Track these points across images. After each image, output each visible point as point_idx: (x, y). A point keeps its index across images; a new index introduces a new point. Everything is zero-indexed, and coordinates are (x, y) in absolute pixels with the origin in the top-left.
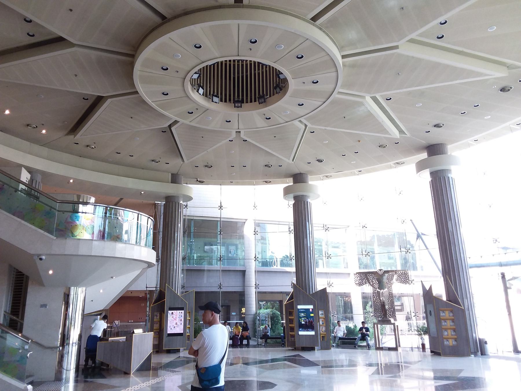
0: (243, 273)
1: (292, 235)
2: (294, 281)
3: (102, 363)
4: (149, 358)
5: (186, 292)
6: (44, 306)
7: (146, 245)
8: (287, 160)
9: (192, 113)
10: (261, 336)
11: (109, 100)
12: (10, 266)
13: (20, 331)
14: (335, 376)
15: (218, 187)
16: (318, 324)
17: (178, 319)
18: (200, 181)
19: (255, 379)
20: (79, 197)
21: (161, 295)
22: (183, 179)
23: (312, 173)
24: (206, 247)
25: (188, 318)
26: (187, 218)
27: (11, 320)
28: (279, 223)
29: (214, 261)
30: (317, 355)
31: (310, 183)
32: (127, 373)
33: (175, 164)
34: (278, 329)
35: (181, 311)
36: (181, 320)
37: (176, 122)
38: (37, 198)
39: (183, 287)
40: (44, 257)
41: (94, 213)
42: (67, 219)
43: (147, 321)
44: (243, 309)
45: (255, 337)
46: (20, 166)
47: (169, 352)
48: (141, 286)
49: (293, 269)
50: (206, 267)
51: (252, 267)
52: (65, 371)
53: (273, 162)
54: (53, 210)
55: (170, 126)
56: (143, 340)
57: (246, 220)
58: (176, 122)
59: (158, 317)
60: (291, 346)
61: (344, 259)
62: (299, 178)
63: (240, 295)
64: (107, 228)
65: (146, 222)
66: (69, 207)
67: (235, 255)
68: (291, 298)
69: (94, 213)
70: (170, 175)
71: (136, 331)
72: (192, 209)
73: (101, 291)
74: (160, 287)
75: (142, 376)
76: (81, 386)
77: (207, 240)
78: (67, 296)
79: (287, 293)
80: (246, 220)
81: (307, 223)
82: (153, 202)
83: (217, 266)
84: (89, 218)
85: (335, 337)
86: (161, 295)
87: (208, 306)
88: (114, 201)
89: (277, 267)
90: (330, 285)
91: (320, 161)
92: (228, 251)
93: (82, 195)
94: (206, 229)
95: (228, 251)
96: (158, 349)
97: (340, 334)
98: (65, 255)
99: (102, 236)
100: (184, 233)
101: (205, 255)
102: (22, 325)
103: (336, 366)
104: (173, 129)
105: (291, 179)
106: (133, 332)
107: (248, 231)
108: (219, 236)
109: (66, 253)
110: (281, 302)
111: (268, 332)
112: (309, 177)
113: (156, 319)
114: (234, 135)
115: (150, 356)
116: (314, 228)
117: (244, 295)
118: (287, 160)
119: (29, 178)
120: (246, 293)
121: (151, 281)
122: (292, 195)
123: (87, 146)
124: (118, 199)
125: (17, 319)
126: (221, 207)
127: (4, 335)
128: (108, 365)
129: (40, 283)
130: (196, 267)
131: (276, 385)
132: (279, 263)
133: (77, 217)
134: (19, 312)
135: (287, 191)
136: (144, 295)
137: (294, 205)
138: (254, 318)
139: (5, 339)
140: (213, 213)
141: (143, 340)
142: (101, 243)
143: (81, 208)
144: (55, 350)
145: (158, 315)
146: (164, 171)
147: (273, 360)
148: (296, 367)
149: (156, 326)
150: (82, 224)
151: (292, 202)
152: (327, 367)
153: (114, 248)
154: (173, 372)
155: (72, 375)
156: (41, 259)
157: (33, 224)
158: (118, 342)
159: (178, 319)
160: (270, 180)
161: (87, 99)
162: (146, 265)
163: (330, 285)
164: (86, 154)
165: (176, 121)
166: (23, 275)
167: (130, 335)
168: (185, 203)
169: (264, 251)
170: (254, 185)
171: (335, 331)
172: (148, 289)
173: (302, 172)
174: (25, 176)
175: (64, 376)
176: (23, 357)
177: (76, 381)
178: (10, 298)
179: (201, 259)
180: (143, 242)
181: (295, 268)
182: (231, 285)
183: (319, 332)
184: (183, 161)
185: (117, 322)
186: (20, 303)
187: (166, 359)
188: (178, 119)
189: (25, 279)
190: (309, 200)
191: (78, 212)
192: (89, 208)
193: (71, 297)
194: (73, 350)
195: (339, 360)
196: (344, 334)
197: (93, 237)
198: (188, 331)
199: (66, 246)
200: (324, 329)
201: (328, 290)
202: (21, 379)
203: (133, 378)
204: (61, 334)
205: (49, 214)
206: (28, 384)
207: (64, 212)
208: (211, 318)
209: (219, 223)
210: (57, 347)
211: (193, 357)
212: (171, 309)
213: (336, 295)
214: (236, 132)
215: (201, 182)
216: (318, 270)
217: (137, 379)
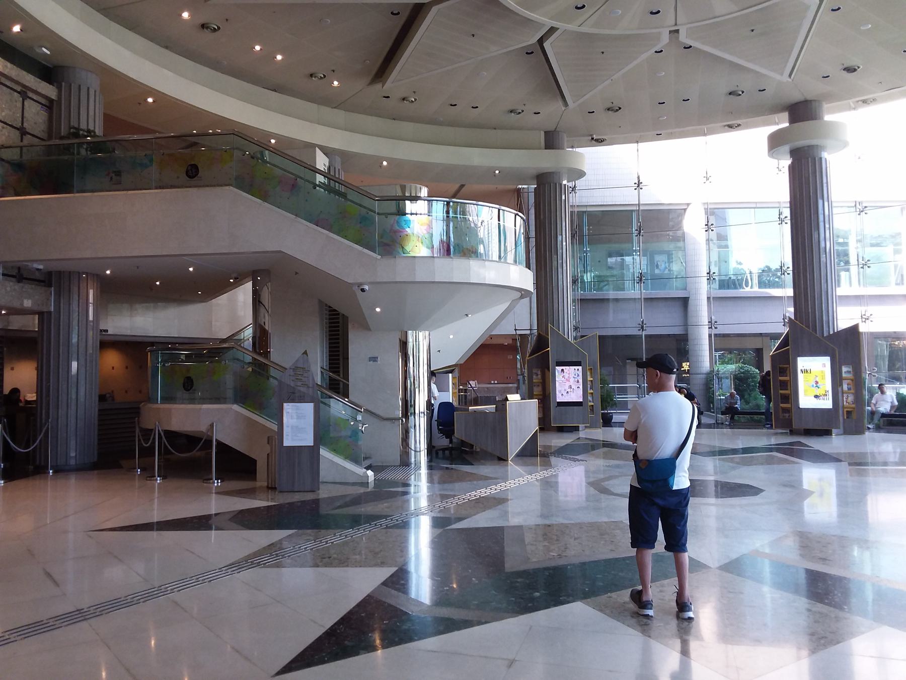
0: (684, 302)
1: (787, 228)
2: (790, 311)
3: (463, 443)
4: (534, 438)
5: (582, 336)
6: (374, 359)
7: (515, 261)
8: (777, 77)
9: (584, 6)
10: (723, 409)
11: (434, 10)
12: (320, 302)
13: (346, 395)
14: (870, 479)
15: (633, 146)
16: (840, 389)
17: (572, 380)
18: (597, 140)
19: (712, 478)
20: (403, 188)
21: (541, 342)
22: (566, 139)
23: (830, 97)
24: (609, 260)
25: (589, 378)
26: (576, 210)
27: (331, 379)
28: (756, 206)
29: (628, 284)
30: (836, 443)
31: (827, 118)
32: (502, 459)
33: (551, 112)
34: (756, 399)
35: (577, 368)
36: (578, 382)
37: (552, 30)
38: (343, 195)
39: (576, 328)
40: (366, 287)
41: (429, 213)
42: (392, 226)
43: (521, 382)
44: (684, 364)
45: (709, 410)
46: (312, 147)
47: (561, 430)
48: (507, 329)
49: (790, 292)
50: (612, 294)
51: (702, 291)
52: (413, 453)
53: (745, 83)
54: (370, 213)
55: (541, 41)
56: (521, 412)
57: (688, 204)
58: (552, 30)
59: (539, 376)
60: (782, 427)
61: (896, 267)
62: (802, 111)
63: (677, 340)
64: (452, 236)
65: (513, 221)
66: (392, 206)
67: (666, 272)
68: (785, 343)
69: (429, 213)
70: (543, 133)
71: (510, 397)
72: (584, 193)
73: (451, 337)
74: (538, 329)
75: (525, 464)
76: (437, 474)
77: (616, 246)
78: (404, 345)
79: (774, 337)
80: (688, 204)
81: (820, 202)
82: (514, 187)
83: (633, 292)
84: (423, 221)
85: (873, 413)
86: (541, 342)
87: (662, 359)
88: (457, 190)
89: (753, 289)
90: (865, 319)
91: (850, 70)
92: (653, 264)
93: (408, 186)
94: (611, 228)
95: (653, 264)
96: (545, 425)
97: (885, 407)
98: (396, 282)
99: (447, 250)
100: (573, 236)
101: (608, 273)
102: (346, 387)
103: (873, 464)
104: (547, 45)
105: (785, 115)
106: (507, 399)
107: (693, 226)
108: (635, 239)
109: (378, 280)
110: (759, 352)
111: (736, 403)
112: (826, 106)
113: (537, 379)
114: (665, 38)
115: (535, 436)
116: (835, 211)
117: (687, 340)
118: (777, 77)
119: (327, 164)
120: (690, 337)
121: (523, 321)
122: (786, 148)
123: (404, 99)
124: (457, 186)
125: (338, 377)
126: (639, 184)
127: (326, 401)
128: (472, 446)
129: (365, 326)
130: (595, 294)
131: (761, 491)
132: (756, 281)
133: (408, 222)
134: (339, 368)
135: (775, 141)
136: (511, 342)
137: (792, 169)
138: (707, 379)
139: (329, 406)
140: (625, 197)
141: (521, 412)
142: (446, 261)
143: (409, 206)
144: (397, 422)
145: (539, 373)
146: (512, 128)
147: (746, 450)
148: (794, 462)
149: (537, 390)
150: (415, 232)
151: (787, 162)
152: (860, 464)
153: (470, 268)
154: (575, 460)
155: (423, 458)
156: (363, 290)
157: (345, 237)
158: (483, 413)
159: (572, 380)
160: (739, 122)
161: (398, 13)
162: (518, 294)
163: (865, 319)
164: (401, 114)
165: (552, 28)
166: (338, 314)
167: (502, 405)
168: (571, 184)
169: (723, 260)
170: (705, 135)
171: (873, 401)
172: (519, 333)
173: (809, 97)
174: (322, 162)
175: (413, 460)
176: (355, 433)
177: (430, 467)
178: (326, 351)
179: (600, 281)
180: (510, 257)
181: (792, 290)
182: (663, 323)
183: (840, 404)
184: (566, 104)
185: (473, 383)
186: (338, 355)
187: (558, 441)
188: (555, 24)
189: (341, 320)
190: (825, 155)
191: (405, 214)
192: (420, 206)
193: (410, 345)
194: (420, 424)
195: (880, 453)
196: (892, 407)
197: (433, 252)
198: (590, 398)
199: (385, 269)
200: (851, 398)
201: (862, 329)
202: (356, 461)
203: (512, 467)
204: (402, 400)
205: (365, 221)
206: (367, 468)
207: (387, 215)
208: (657, 381)
209: (634, 215)
210: (399, 419)
211: (631, 443)
212: (560, 364)
213: (876, 336)
214: (670, 32)
215: (600, 142)
216: (840, 291)
217: (519, 469)
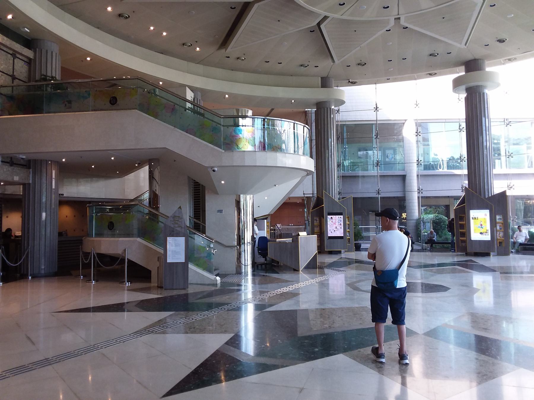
0: (403, 178)
1: (464, 134)
2: (466, 183)
3: (273, 261)
4: (315, 257)
5: (343, 198)
6: (220, 211)
7: (304, 154)
8: (458, 45)
9: (344, 4)
10: (426, 241)
11: (256, 6)
12: (189, 177)
13: (204, 232)
14: (513, 282)
15: (373, 86)
16: (495, 229)
17: (337, 223)
18: (352, 83)
19: (420, 281)
20: (238, 111)
21: (319, 201)
22: (333, 82)
23: (489, 57)
24: (359, 153)
25: (347, 223)
26: (340, 123)
27: (195, 223)
28: (446, 121)
29: (370, 167)
30: (493, 261)
31: (488, 69)
32: (296, 270)
33: (324, 66)
34: (445, 235)
35: (340, 216)
36: (341, 224)
37: (326, 18)
38: (202, 115)
39: (339, 193)
40: (216, 169)
41: (253, 125)
42: (231, 133)
43: (307, 224)
44: (403, 214)
45: (418, 241)
46: (184, 86)
47: (331, 253)
48: (299, 193)
49: (466, 172)
50: (361, 173)
51: (414, 171)
52: (243, 266)
53: (439, 49)
54: (218, 125)
55: (319, 24)
56: (307, 242)
57: (406, 120)
58: (326, 18)
59: (318, 221)
60: (461, 251)
61: (528, 157)
62: (472, 65)
63: (399, 200)
64: (266, 139)
65: (302, 130)
66: (231, 121)
67: (393, 160)
68: (463, 201)
69: (253, 125)
70: (320, 78)
71: (301, 233)
72: (344, 114)
73: (266, 198)
74: (317, 194)
75: (309, 273)
76: (258, 279)
77: (363, 145)
78: (238, 203)
79: (456, 198)
80: (406, 120)
81: (483, 119)
82: (303, 110)
83: (373, 171)
84: (249, 130)
85: (514, 243)
86: (319, 201)
87: (390, 211)
88: (269, 112)
89: (444, 170)
90: (510, 187)
91: (501, 41)
92: (385, 155)
93: (240, 109)
94: (360, 134)
95: (385, 155)
96: (321, 250)
97: (521, 239)
98: (234, 166)
99: (263, 147)
100: (338, 139)
101: (358, 161)
102: (204, 227)
103: (515, 273)
104: (322, 26)
105: (463, 68)
106: (299, 235)
107: (408, 133)
108: (374, 140)
109: (223, 165)
110: (447, 207)
111: (434, 237)
112: (487, 62)
113: (316, 223)
114: (392, 22)
115: (315, 256)
116: (492, 124)
117: (405, 200)
118: (458, 45)
119: (193, 97)
120: (407, 198)
121: (308, 189)
122: (464, 87)
123: (238, 58)
124: (269, 109)
125: (199, 222)
126: (376, 108)
127: (192, 236)
128: (278, 262)
129: (215, 192)
130: (350, 173)
131: (449, 289)
132: (445, 165)
133: (240, 131)
134: (200, 216)
135: (457, 83)
136: (301, 201)
137: (467, 99)
138: (416, 223)
139: (194, 239)
140: (368, 116)
141: (307, 242)
142: (263, 154)
143: (241, 121)
144: (234, 248)
145: (318, 219)
146: (302, 75)
147: (439, 265)
148: (468, 272)
149: (317, 230)
150: (245, 137)
151: (464, 95)
152: (507, 273)
153: (277, 157)
154: (339, 271)
155: (249, 269)
156: (214, 171)
157: (203, 140)
158: (285, 243)
159: (337, 223)
160: (435, 72)
161: (235, 8)
162: (305, 173)
163: (510, 187)
164: (236, 67)
165: (325, 16)
166: (199, 185)
167: (296, 238)
168: (336, 108)
169: (426, 153)
170: (415, 79)
171: (515, 236)
172: (306, 196)
173: (477, 57)
174: (190, 95)
175: (243, 270)
176: (209, 254)
177: (253, 275)
178: (192, 206)
179: (354, 165)
180: (301, 151)
181: (467, 171)
182: (391, 190)
183: (495, 238)
184: (334, 61)
185: (279, 225)
186: (199, 209)
187: (329, 259)
188: (327, 14)
189: (201, 188)
190: (486, 91)
191: (239, 126)
192: (248, 121)
193: (242, 203)
194: (248, 249)
195: (519, 267)
196: (526, 239)
197: (255, 148)
198: (348, 234)
199: (227, 158)
200: (502, 234)
201: (508, 193)
202: (210, 271)
203: (302, 275)
204: (237, 235)
205: (215, 130)
206: (217, 275)
207: (228, 126)
208: (387, 224)
209: (374, 127)
210: (235, 246)
211: (372, 261)
212: (330, 214)
213: (516, 198)
214: (395, 19)
215: (354, 83)
216: (495, 171)
217: (306, 276)
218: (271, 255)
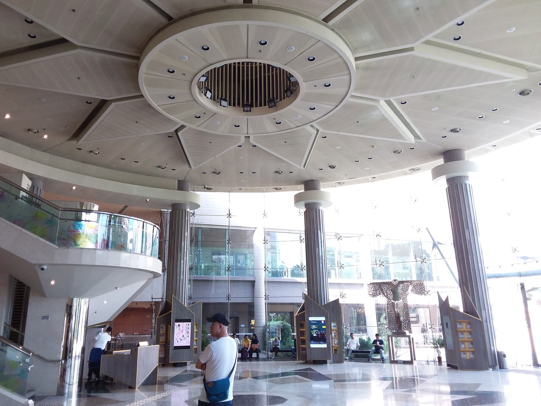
0: (253, 283)
1: (304, 245)
2: (306, 292)
3: (106, 377)
4: (155, 372)
5: (193, 303)
6: (46, 317)
7: (151, 254)
8: (298, 167)
9: (200, 117)
10: (272, 349)
11: (113, 104)
12: (11, 276)
13: (21, 343)
14: (348, 390)
15: (227, 194)
16: (330, 336)
17: (184, 331)
18: (207, 188)
19: (265, 394)
20: (82, 204)
21: (167, 307)
22: (190, 186)
23: (324, 180)
24: (214, 257)
25: (195, 330)
26: (194, 226)
27: (12, 332)
28: (290, 232)
29: (222, 271)
30: (329, 369)
31: (322, 190)
32: (132, 387)
33: (181, 170)
34: (289, 342)
35: (188, 323)
36: (188, 332)
37: (183, 127)
38: (39, 206)
39: (190, 298)
40: (45, 267)
41: (98, 222)
42: (69, 227)
43: (153, 334)
44: (252, 321)
45: (264, 350)
46: (21, 172)
47: (175, 365)
48: (146, 297)
49: (305, 280)
50: (214, 277)
51: (262, 277)
52: (67, 385)
53: (283, 168)
54: (55, 218)
55: (177, 131)
56: (148, 353)
57: (256, 228)
58: (183, 127)
59: (164, 329)
60: (302, 359)
61: (357, 269)
62: (310, 185)
63: (249, 306)
64: (111, 236)
65: (152, 230)
66: (72, 215)
67: (244, 265)
68: (303, 309)
69: (98, 222)
70: (177, 181)
71: (141, 344)
72: (200, 217)
73: (105, 302)
74: (166, 298)
75: (147, 390)
76: (84, 400)
77: (215, 249)
78: (69, 308)
79: (298, 305)
80: (256, 228)
81: (319, 232)
82: (159, 210)
83: (225, 276)
84: (93, 227)
85: (348, 350)
86: (167, 307)
87: (216, 318)
88: (118, 209)
89: (288, 278)
90: (343, 296)
91: (332, 167)
92: (237, 261)
93: (85, 203)
94: (214, 238)
95: (237, 261)
96: (164, 362)
97: (353, 347)
98: (68, 265)
99: (106, 245)
100: (191, 241)
101: (213, 264)
102: (23, 337)
103: (349, 381)
104: (179, 134)
105: (302, 186)
106: (139, 345)
107: (258, 240)
108: (227, 245)
109: (69, 263)
110: (292, 313)
111: (278, 345)
112: (321, 184)
113: (162, 331)
114: (243, 140)
115: (156, 370)
116: (326, 237)
117: (253, 306)
118: (298, 167)
119: (30, 185)
120: (255, 304)
121: (156, 292)
122: (303, 203)
123: (91, 152)
124: (123, 206)
125: (18, 331)
126: (229, 215)
127: (4, 348)
128: (112, 379)
129: (42, 294)
130: (203, 277)
131: (286, 400)
132: (289, 273)
133: (80, 226)
134: (19, 324)
135: (298, 199)
136: (149, 306)
137: (306, 213)
138: (264, 330)
139: (6, 352)
140: (221, 221)
141: (148, 353)
142: (105, 253)
143: (84, 216)
144: (57, 364)
145: (164, 327)
146: (170, 178)
147: (283, 374)
148: (307, 381)
149: (162, 339)
150: (85, 233)
151: (304, 210)
152: (340, 381)
153: (118, 257)
154: (180, 386)
155: (75, 389)
156: (42, 269)
157: (34, 233)
158: (122, 355)
159: (184, 331)
160: (281, 187)
161: (91, 103)
162: (152, 275)
163: (343, 296)
164: (89, 160)
165: (182, 125)
166: (24, 285)
167: (135, 347)
168: (192, 211)
169: (274, 261)
170: (264, 192)
171: (348, 343)
172: (154, 300)
173: (314, 179)
174: (26, 183)
175: (67, 391)
176: (24, 371)
177: (79, 396)
178: (11, 309)
179: (208, 269)
180: (149, 252)
181: (306, 279)
182: (240, 296)
183: (331, 345)
184: (190, 167)
185: (121, 335)
186: (20, 315)
187: (172, 373)
188: (185, 124)
189: (25, 290)
190: (321, 208)
191: (81, 220)
192: (92, 216)
193: (74, 308)
194: (75, 364)
195: (352, 374)
196: (357, 347)
197: (96, 246)
198: (195, 343)
199: (69, 256)
200: (336, 342)
201: (341, 301)
202: (22, 393)
203: (138, 392)
204: (64, 347)
205: (51, 222)
206: (29, 399)
207: (66, 220)
208: (220, 331)
209: (227, 232)
210: (60, 361)
211: (200, 370)
212: (177, 321)
213: (349, 306)
214: (245, 137)
215: (209, 189)
216: (330, 281)
217: (143, 394)
218: (103, 372)
